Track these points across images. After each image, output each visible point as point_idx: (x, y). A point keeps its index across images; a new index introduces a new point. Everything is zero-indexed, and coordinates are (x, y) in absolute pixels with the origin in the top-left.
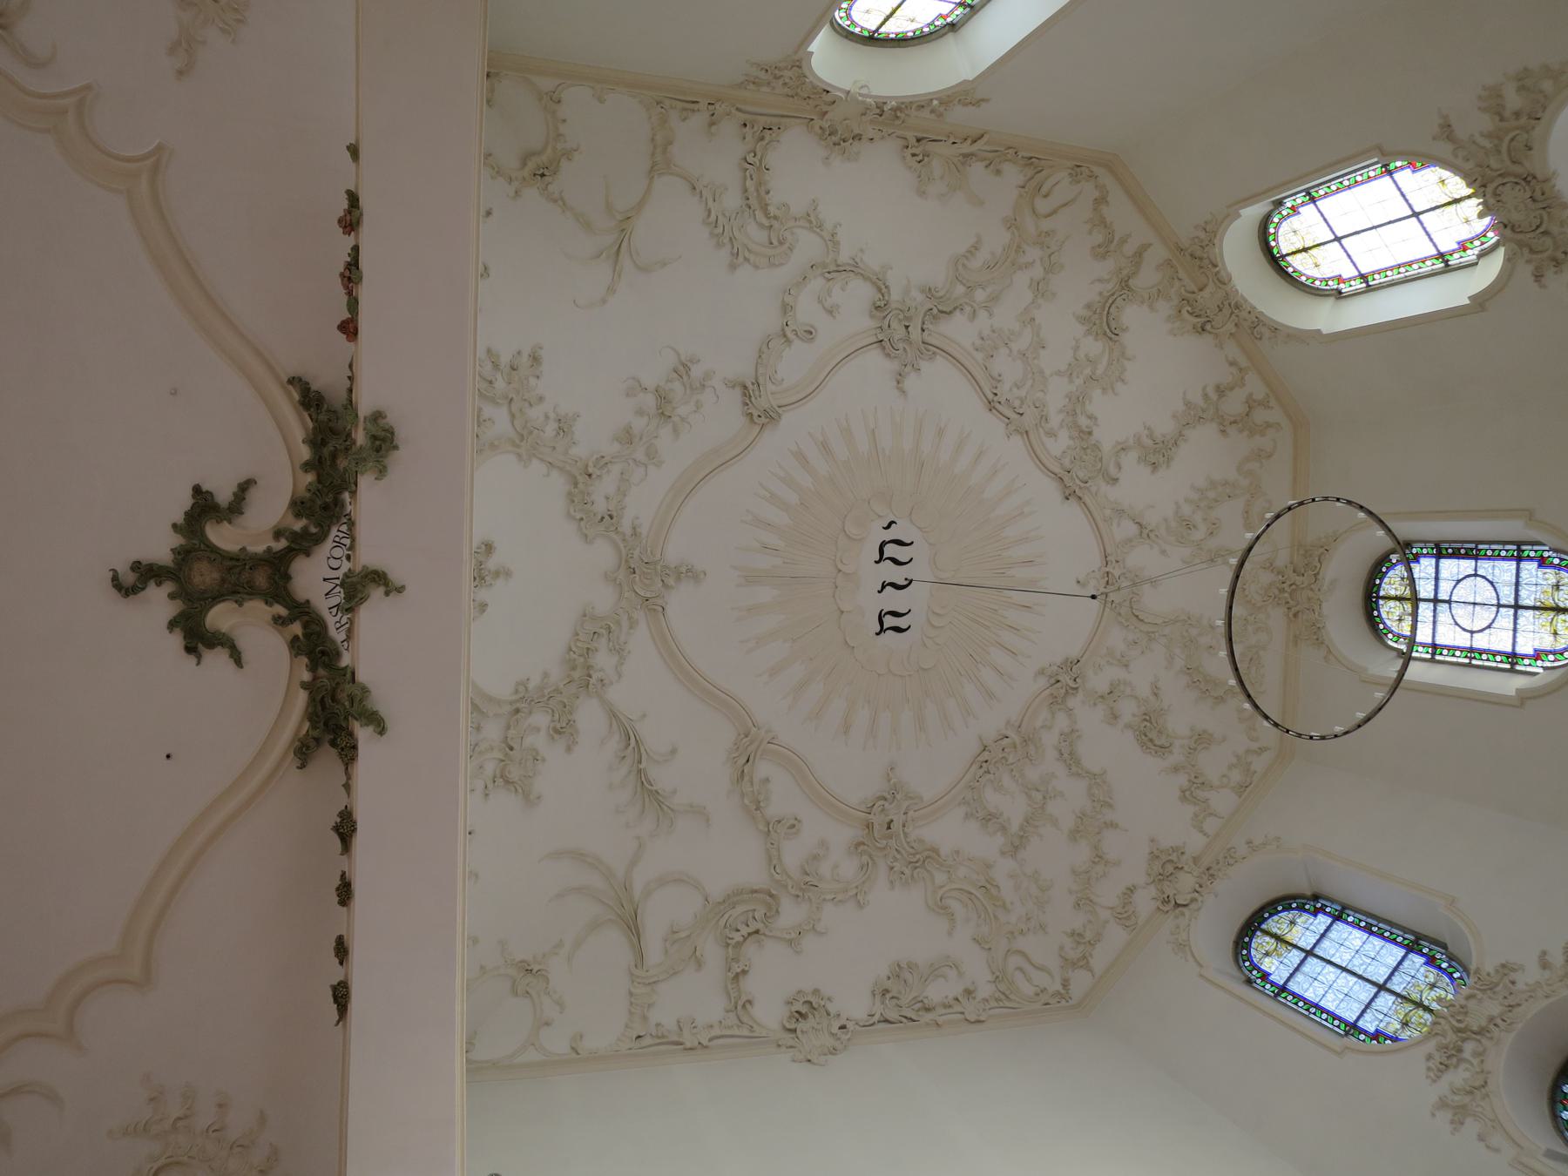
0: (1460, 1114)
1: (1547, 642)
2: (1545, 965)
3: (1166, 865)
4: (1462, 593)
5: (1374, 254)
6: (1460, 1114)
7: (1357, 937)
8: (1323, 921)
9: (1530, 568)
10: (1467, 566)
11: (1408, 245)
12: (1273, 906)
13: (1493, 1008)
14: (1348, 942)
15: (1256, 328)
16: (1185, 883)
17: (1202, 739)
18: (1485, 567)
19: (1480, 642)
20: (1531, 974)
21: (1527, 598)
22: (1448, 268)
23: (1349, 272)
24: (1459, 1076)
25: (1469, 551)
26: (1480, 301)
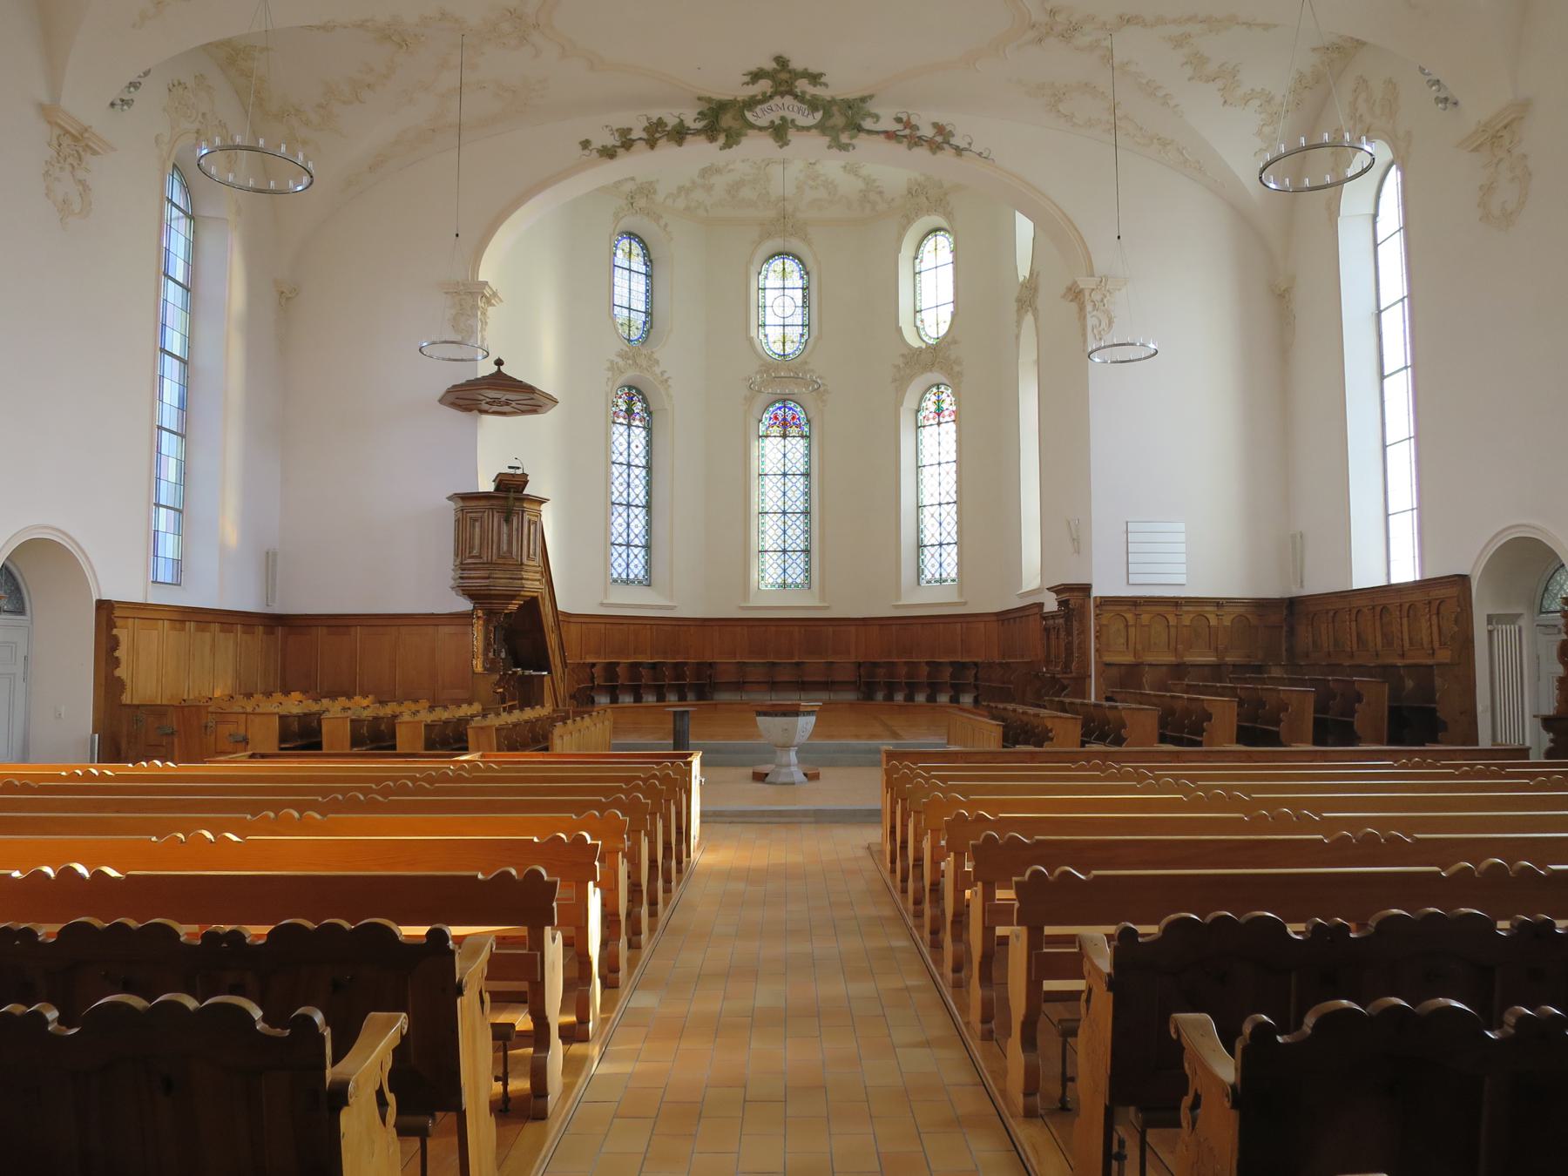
0: (611, 369)
1: (771, 339)
2: (663, 373)
3: (647, 190)
4: (788, 301)
5: (926, 280)
6: (611, 369)
7: (642, 288)
8: (643, 269)
9: (799, 330)
10: (799, 302)
11: (926, 301)
12: (641, 241)
13: (644, 364)
14: (640, 284)
15: (908, 221)
16: (641, 202)
17: (709, 188)
18: (799, 311)
19: (768, 310)
20: (658, 370)
21: (779, 284)
22: (916, 312)
23: (924, 266)
24: (621, 363)
25: (806, 302)
26: (899, 330)
